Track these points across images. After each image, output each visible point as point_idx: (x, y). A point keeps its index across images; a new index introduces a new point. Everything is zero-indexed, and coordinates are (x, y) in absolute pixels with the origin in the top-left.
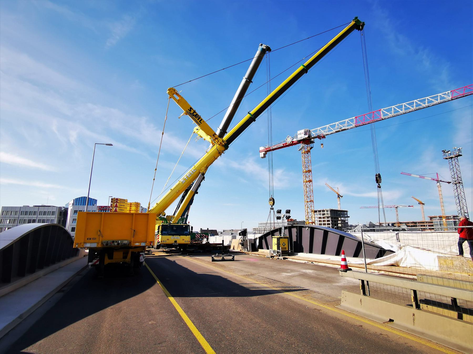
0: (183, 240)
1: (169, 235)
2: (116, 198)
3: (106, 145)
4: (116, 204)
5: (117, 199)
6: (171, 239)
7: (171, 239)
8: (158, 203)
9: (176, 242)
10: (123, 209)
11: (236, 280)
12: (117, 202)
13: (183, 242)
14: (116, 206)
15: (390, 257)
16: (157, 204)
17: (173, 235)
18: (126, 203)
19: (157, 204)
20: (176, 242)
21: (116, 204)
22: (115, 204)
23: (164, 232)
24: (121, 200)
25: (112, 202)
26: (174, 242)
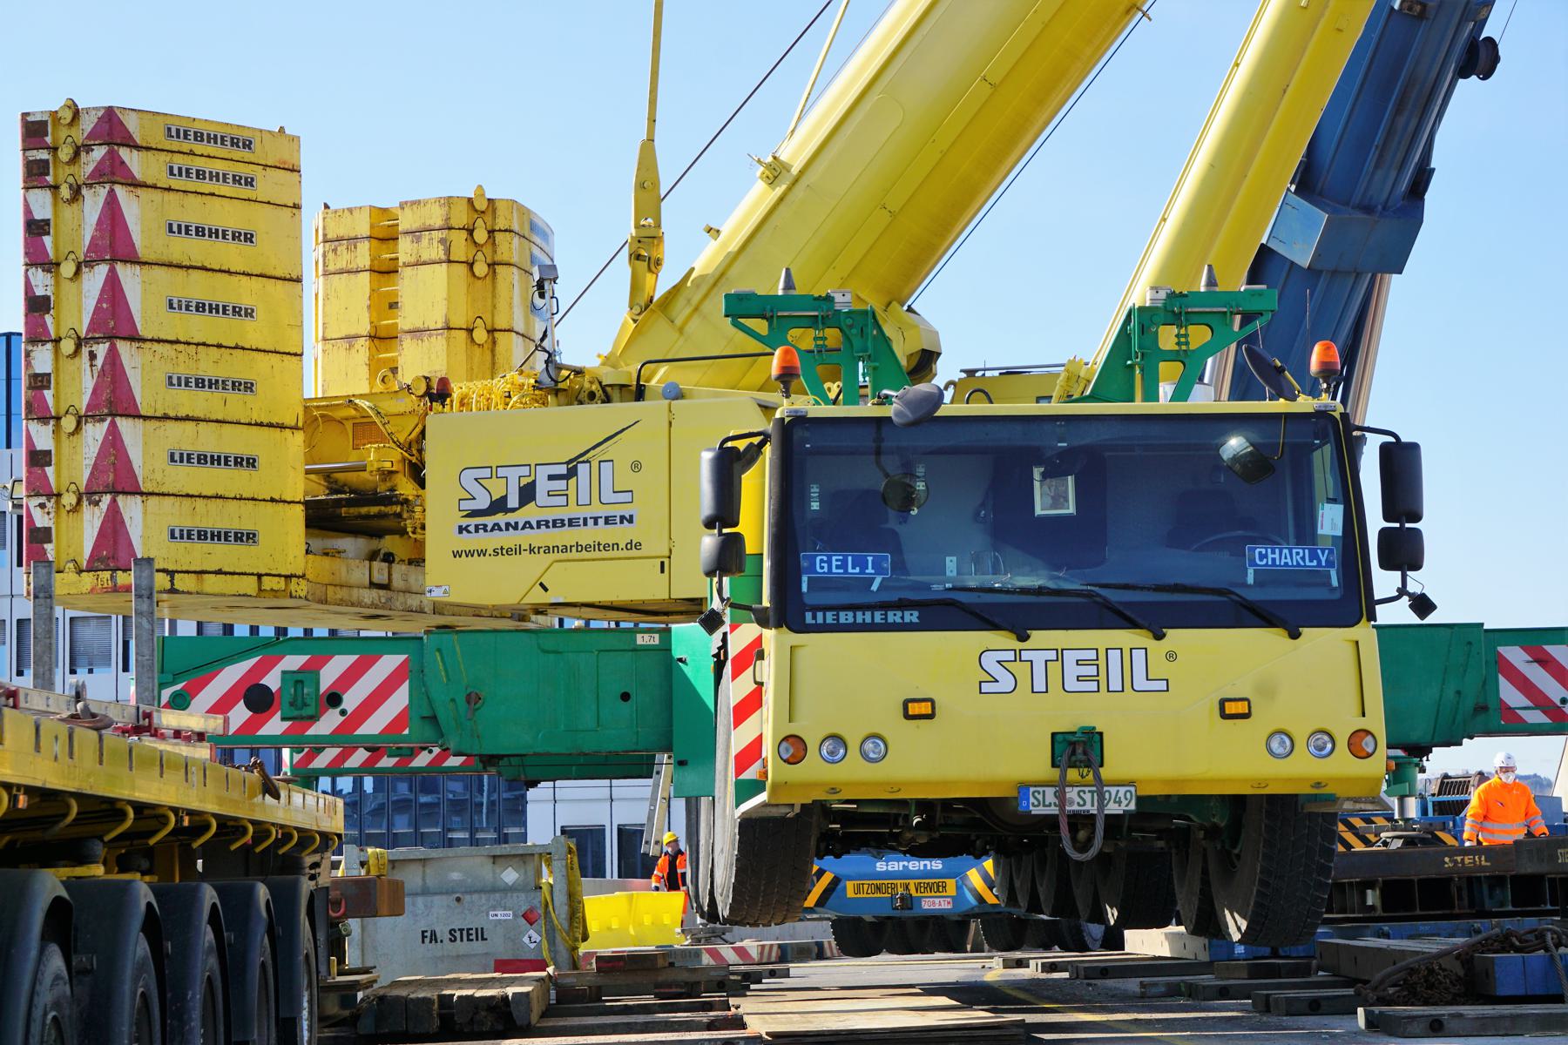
0: (1231, 711)
1: (946, 612)
2: (93, 98)
3: (649, 144)
4: (112, 215)
5: (112, 128)
6: (966, 709)
7: (966, 709)
8: (794, 152)
9: (1078, 749)
10: (243, 292)
11: (945, 784)
12: (113, 172)
13: (1232, 763)
14: (114, 244)
15: (1513, 1018)
16: (775, 171)
17: (1016, 616)
18: (268, 185)
19: (775, 171)
20: (1078, 749)
21: (112, 215)
22: (94, 201)
23: (826, 564)
24: (184, 133)
25: (35, 174)
26: (1035, 763)
